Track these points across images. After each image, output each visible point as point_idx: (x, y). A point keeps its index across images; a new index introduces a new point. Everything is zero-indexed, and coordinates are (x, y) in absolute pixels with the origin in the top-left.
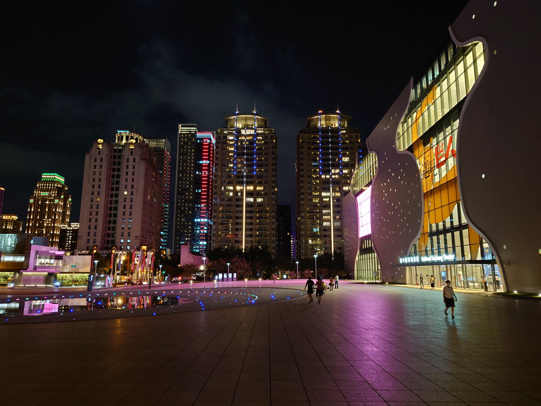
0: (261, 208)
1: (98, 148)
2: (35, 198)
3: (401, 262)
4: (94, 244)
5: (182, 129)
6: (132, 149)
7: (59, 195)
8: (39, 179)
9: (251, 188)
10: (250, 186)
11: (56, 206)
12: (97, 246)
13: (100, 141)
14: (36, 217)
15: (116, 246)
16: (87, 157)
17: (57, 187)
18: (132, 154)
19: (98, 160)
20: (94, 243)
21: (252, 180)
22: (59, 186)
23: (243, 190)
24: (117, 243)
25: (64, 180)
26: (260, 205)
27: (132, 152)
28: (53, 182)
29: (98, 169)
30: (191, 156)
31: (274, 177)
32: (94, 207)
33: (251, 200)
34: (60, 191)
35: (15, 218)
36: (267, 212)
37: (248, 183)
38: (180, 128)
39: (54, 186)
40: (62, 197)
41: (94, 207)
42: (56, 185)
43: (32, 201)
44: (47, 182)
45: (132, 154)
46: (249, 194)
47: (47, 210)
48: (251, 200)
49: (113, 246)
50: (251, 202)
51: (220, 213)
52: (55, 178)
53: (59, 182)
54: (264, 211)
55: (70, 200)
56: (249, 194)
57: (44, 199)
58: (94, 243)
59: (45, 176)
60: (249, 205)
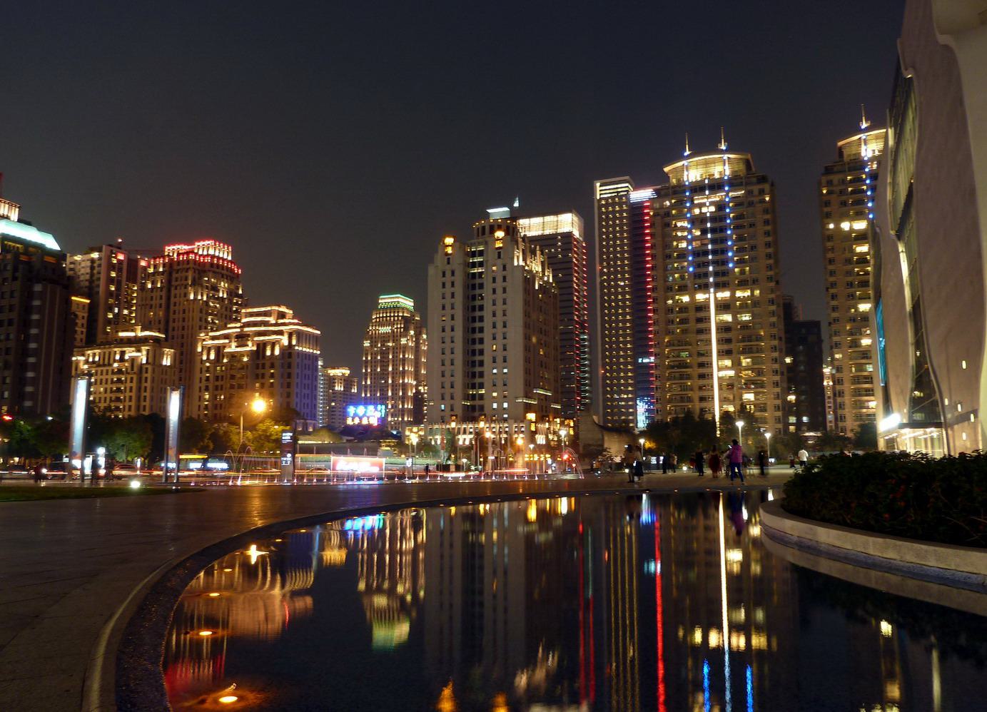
0: (747, 332)
1: (447, 254)
2: (371, 338)
3: (656, 463)
4: (452, 413)
5: (602, 191)
6: (500, 248)
7: (406, 329)
8: (374, 305)
9: (727, 294)
10: (723, 291)
11: (405, 349)
12: (456, 416)
13: (449, 241)
14: (375, 370)
15: (485, 415)
16: (431, 271)
17: (403, 317)
18: (499, 257)
19: (448, 273)
20: (452, 410)
21: (725, 279)
22: (405, 315)
23: (709, 299)
24: (486, 410)
25: (412, 304)
26: (745, 326)
27: (499, 253)
28: (396, 308)
29: (449, 289)
30: (622, 239)
31: (771, 270)
32: (500, 337)
33: (728, 318)
34: (407, 322)
35: (347, 372)
36: (759, 338)
37: (719, 286)
38: (598, 188)
39: (398, 316)
40: (412, 332)
41: (500, 337)
42: (400, 314)
43: (367, 344)
44: (385, 309)
45: (499, 257)
46: (723, 307)
47: (391, 357)
48: (728, 318)
49: (481, 415)
50: (728, 322)
51: (667, 346)
52: (398, 302)
53: (404, 309)
54: (754, 337)
55: (425, 336)
56: (723, 307)
57: (385, 338)
58: (452, 410)
59: (385, 300)
60: (724, 328)
